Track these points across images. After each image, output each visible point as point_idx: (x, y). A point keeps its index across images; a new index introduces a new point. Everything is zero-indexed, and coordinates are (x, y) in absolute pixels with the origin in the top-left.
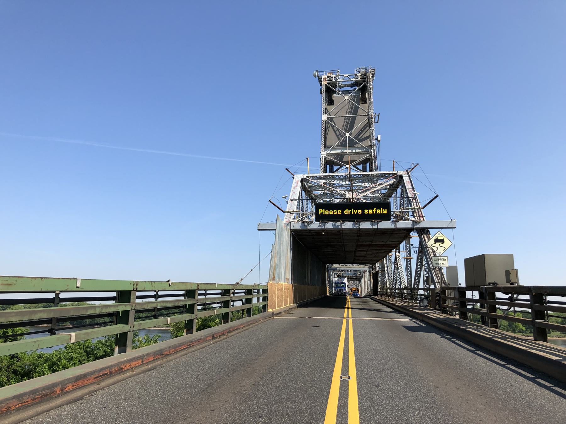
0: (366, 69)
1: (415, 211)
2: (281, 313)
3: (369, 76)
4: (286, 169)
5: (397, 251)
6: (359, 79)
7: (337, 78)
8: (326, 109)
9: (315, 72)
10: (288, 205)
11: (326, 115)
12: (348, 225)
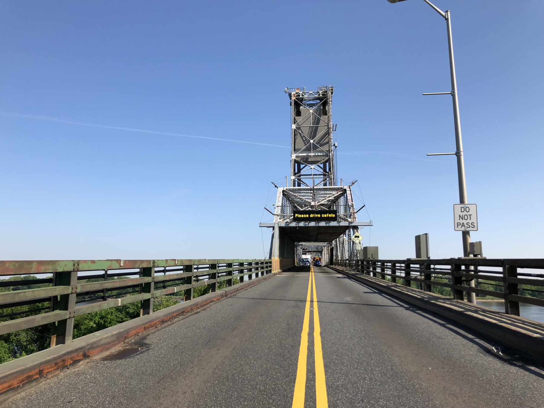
0: (326, 87)
1: (351, 214)
2: (277, 274)
3: (329, 94)
4: (272, 182)
5: (344, 235)
6: (321, 96)
7: (304, 94)
8: (294, 118)
9: (286, 89)
10: (276, 209)
11: (295, 125)
12: (313, 224)
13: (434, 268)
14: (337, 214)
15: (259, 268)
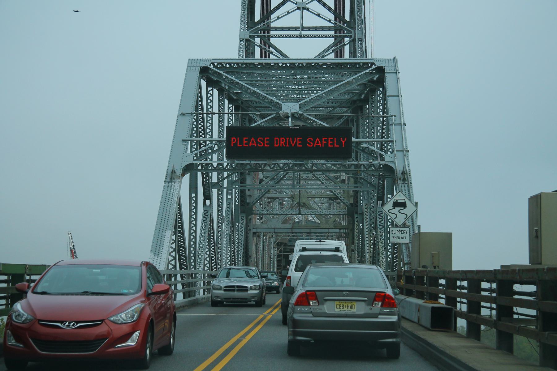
11: (249, 32)
13: (491, 288)
14: (354, 139)
15: (173, 275)
